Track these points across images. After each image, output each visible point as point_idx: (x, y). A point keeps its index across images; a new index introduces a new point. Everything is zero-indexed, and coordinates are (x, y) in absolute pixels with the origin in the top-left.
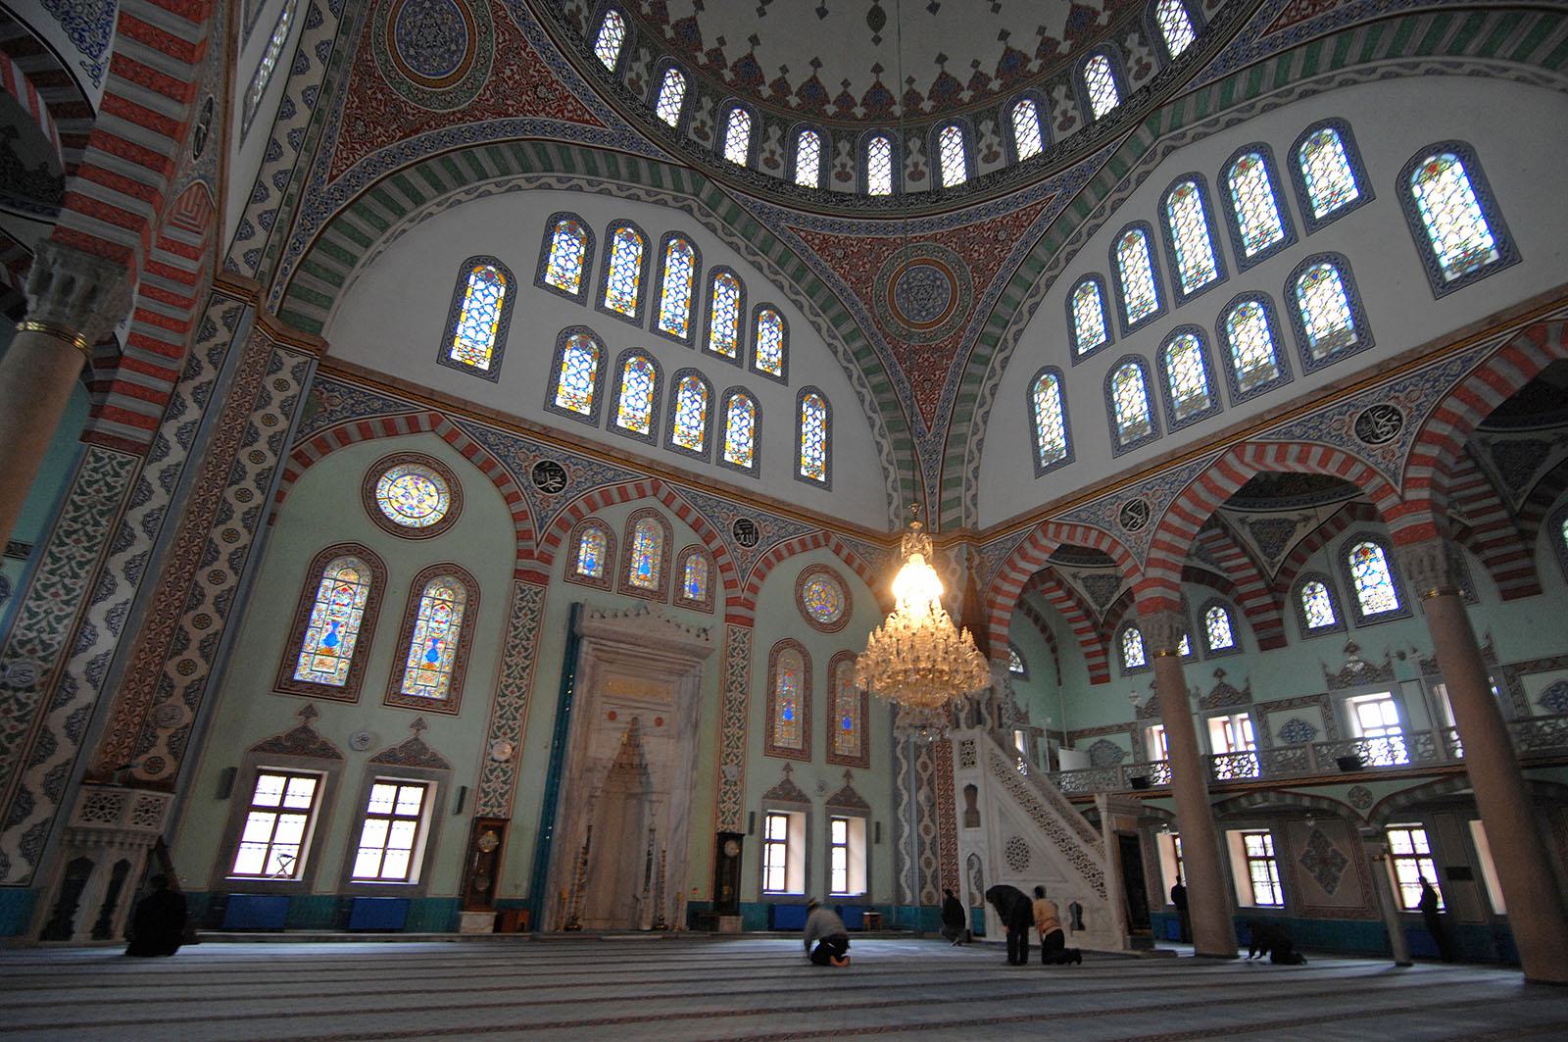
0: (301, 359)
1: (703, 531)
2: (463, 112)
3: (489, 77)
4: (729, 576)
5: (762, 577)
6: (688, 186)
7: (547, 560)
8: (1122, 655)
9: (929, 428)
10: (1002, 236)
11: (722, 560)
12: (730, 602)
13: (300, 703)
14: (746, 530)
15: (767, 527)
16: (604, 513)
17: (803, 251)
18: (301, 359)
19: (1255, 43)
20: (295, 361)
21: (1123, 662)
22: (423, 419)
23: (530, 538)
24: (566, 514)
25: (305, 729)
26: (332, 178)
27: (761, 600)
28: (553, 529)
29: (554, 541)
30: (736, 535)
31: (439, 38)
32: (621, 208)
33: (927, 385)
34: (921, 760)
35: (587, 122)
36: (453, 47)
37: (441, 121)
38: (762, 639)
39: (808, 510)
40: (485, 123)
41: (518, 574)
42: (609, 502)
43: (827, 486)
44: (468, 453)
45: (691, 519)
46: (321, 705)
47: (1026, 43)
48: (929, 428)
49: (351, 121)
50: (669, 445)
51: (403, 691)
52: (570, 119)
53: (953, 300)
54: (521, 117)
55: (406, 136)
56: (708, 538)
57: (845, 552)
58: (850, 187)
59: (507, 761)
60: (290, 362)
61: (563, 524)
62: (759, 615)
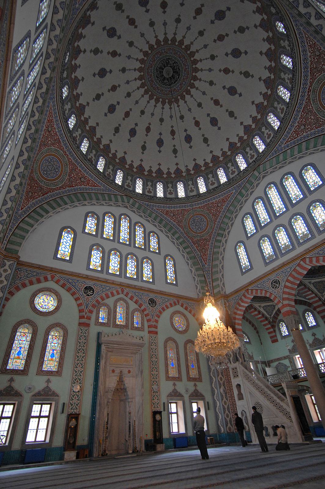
0: (12, 262)
1: (139, 303)
2: (60, 187)
3: (67, 177)
4: (148, 317)
5: (159, 317)
6: (126, 200)
7: (89, 318)
8: (280, 332)
9: (206, 264)
10: (219, 205)
11: (145, 313)
12: (149, 327)
13: (45, 378)
14: (152, 302)
15: (159, 299)
16: (107, 301)
17: (161, 215)
18: (12, 262)
19: (283, 146)
20: (9, 263)
21: (281, 334)
22: (49, 277)
23: (84, 311)
24: (94, 302)
25: (10, 386)
26: (22, 209)
27: (160, 325)
28: (91, 308)
29: (91, 312)
30: (149, 304)
31: (53, 168)
32: (125, 211)
33: (203, 250)
34: (219, 377)
35: (96, 186)
36: (57, 170)
37: (53, 190)
38: (161, 338)
39: (171, 293)
40: (66, 189)
41: (80, 324)
42: (108, 297)
43: (176, 285)
44: (63, 286)
45: (134, 300)
46: (16, 377)
47: (219, 153)
48: (206, 264)
49: (27, 192)
50: (143, 281)
51: (43, 369)
52: (91, 186)
53: (208, 224)
54: (77, 187)
55: (43, 195)
56: (140, 306)
57: (185, 306)
58: (173, 196)
59: (78, 392)
60: (8, 263)
61: (94, 306)
62: (159, 330)
